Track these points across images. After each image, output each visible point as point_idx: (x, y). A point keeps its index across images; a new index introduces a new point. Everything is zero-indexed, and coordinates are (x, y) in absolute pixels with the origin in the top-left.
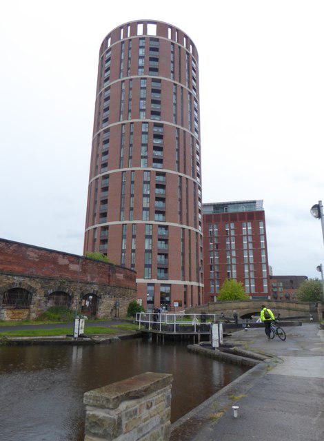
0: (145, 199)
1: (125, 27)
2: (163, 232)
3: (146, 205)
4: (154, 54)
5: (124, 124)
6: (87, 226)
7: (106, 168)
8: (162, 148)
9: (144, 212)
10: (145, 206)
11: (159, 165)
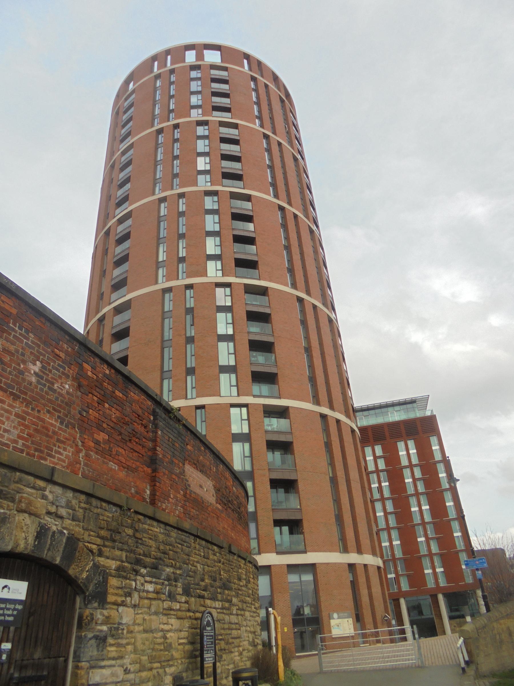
0: (221, 317)
5: (169, 290)
8: (254, 239)
9: (224, 378)
10: (235, 429)
11: (265, 388)
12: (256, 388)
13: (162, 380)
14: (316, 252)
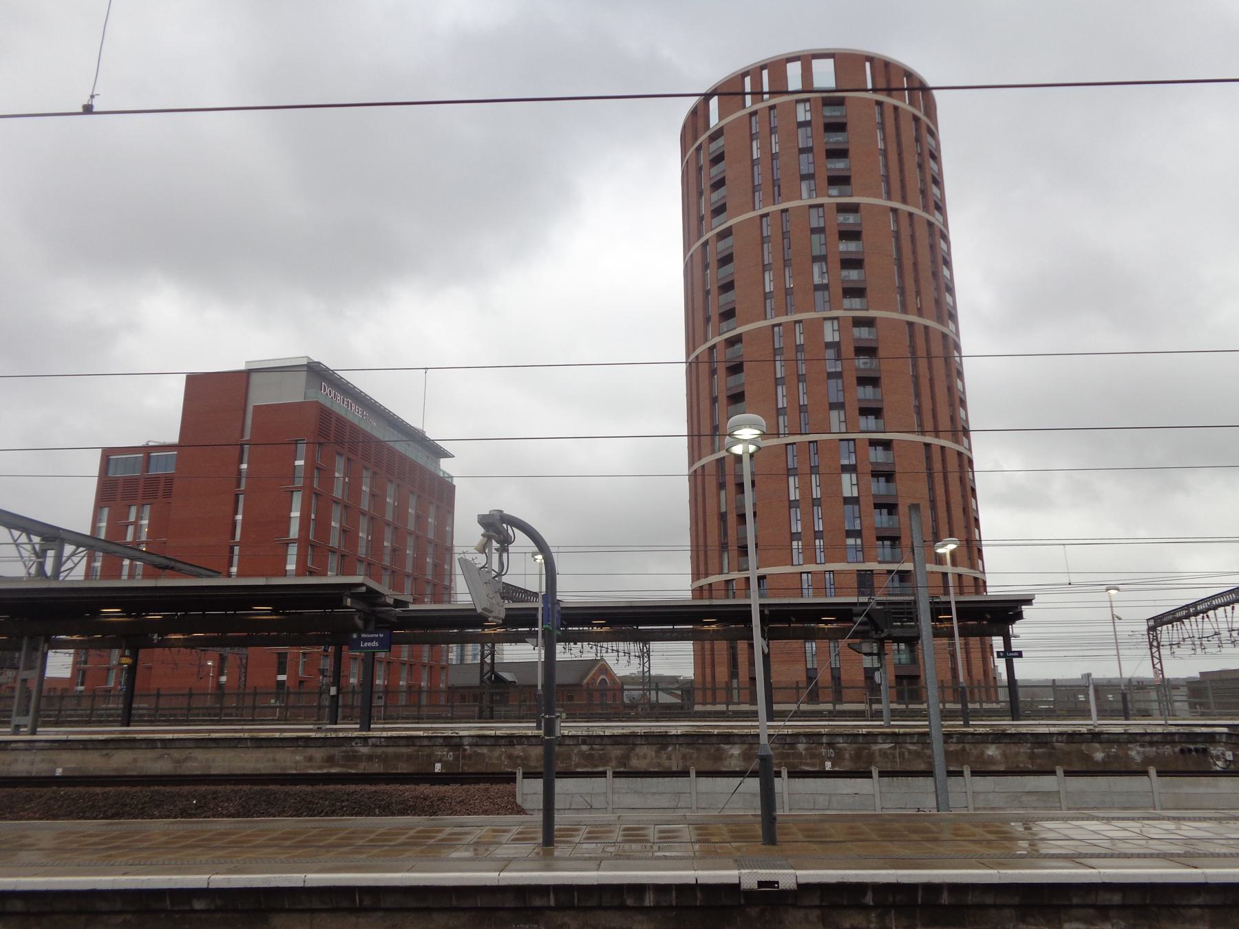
0: (846, 478)
1: (755, 72)
2: (878, 455)
3: (832, 367)
4: (849, 247)
6: (692, 462)
7: (723, 216)
11: (856, 302)
12: (847, 302)
13: (754, 193)
14: (933, 247)
